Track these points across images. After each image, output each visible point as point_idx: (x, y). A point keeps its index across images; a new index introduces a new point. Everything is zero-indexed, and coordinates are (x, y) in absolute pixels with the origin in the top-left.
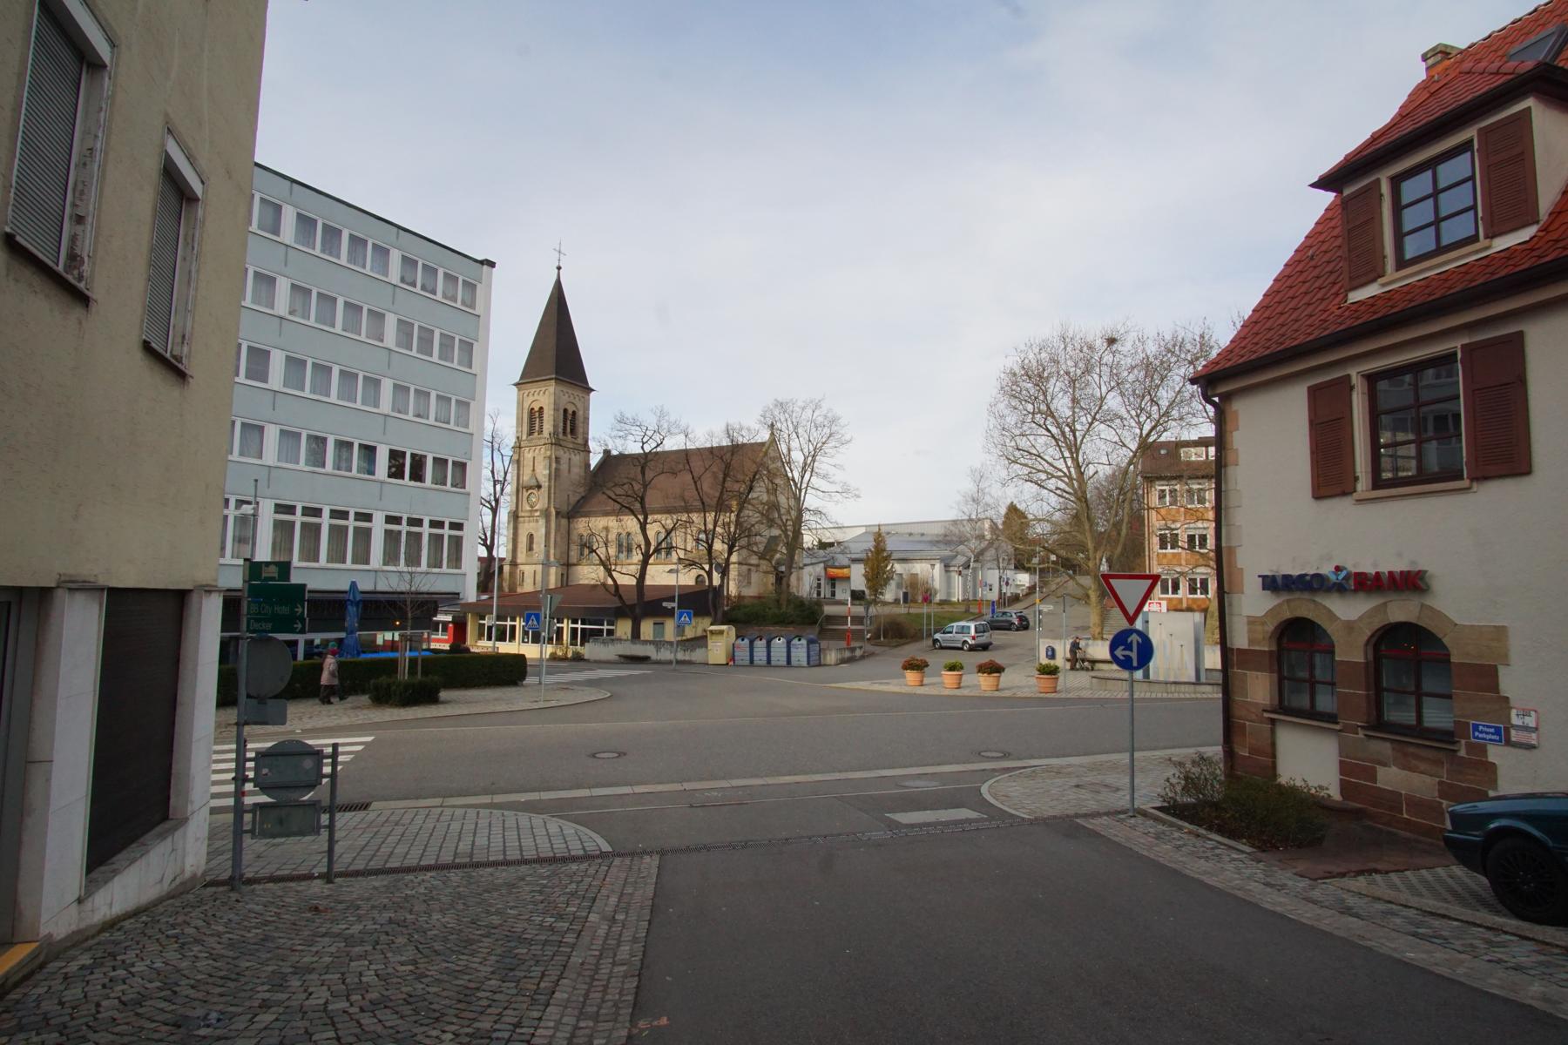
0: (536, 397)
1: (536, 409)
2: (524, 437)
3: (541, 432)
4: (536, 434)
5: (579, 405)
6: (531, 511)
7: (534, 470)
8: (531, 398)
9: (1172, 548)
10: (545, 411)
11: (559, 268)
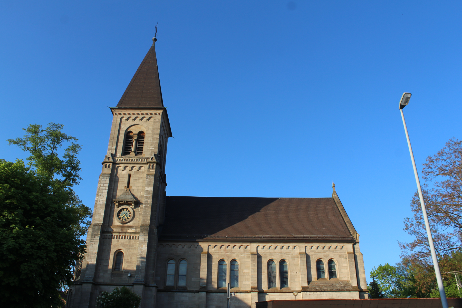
2: (119, 154)
3: (139, 151)
4: (132, 154)
6: (122, 227)
7: (128, 186)
8: (131, 122)
11: (155, 40)
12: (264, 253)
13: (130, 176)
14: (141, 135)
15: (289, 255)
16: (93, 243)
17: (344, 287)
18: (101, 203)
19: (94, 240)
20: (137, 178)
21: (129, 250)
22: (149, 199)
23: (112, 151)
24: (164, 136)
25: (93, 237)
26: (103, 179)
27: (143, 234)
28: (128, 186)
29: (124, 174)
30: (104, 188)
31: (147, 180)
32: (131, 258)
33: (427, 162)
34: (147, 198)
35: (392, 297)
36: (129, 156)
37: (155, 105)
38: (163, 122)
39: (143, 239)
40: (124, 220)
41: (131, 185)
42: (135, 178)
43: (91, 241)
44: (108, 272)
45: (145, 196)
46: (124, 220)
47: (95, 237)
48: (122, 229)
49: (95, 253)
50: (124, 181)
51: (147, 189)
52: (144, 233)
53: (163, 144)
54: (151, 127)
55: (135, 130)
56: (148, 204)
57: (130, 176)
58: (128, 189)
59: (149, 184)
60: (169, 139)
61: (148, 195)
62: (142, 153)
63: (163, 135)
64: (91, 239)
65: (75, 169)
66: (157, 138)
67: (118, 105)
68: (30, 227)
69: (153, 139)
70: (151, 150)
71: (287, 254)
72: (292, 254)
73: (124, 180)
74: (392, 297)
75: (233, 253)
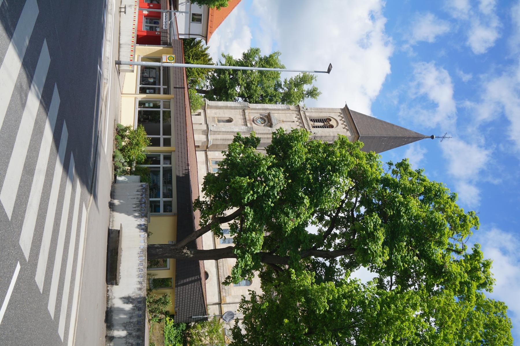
0: (340, 122)
1: (331, 123)
7: (283, 121)
8: (338, 119)
9: (164, 89)
13: (294, 122)
14: (332, 127)
41: (285, 123)
48: (248, 120)
55: (333, 122)
57: (294, 122)
69: (329, 132)
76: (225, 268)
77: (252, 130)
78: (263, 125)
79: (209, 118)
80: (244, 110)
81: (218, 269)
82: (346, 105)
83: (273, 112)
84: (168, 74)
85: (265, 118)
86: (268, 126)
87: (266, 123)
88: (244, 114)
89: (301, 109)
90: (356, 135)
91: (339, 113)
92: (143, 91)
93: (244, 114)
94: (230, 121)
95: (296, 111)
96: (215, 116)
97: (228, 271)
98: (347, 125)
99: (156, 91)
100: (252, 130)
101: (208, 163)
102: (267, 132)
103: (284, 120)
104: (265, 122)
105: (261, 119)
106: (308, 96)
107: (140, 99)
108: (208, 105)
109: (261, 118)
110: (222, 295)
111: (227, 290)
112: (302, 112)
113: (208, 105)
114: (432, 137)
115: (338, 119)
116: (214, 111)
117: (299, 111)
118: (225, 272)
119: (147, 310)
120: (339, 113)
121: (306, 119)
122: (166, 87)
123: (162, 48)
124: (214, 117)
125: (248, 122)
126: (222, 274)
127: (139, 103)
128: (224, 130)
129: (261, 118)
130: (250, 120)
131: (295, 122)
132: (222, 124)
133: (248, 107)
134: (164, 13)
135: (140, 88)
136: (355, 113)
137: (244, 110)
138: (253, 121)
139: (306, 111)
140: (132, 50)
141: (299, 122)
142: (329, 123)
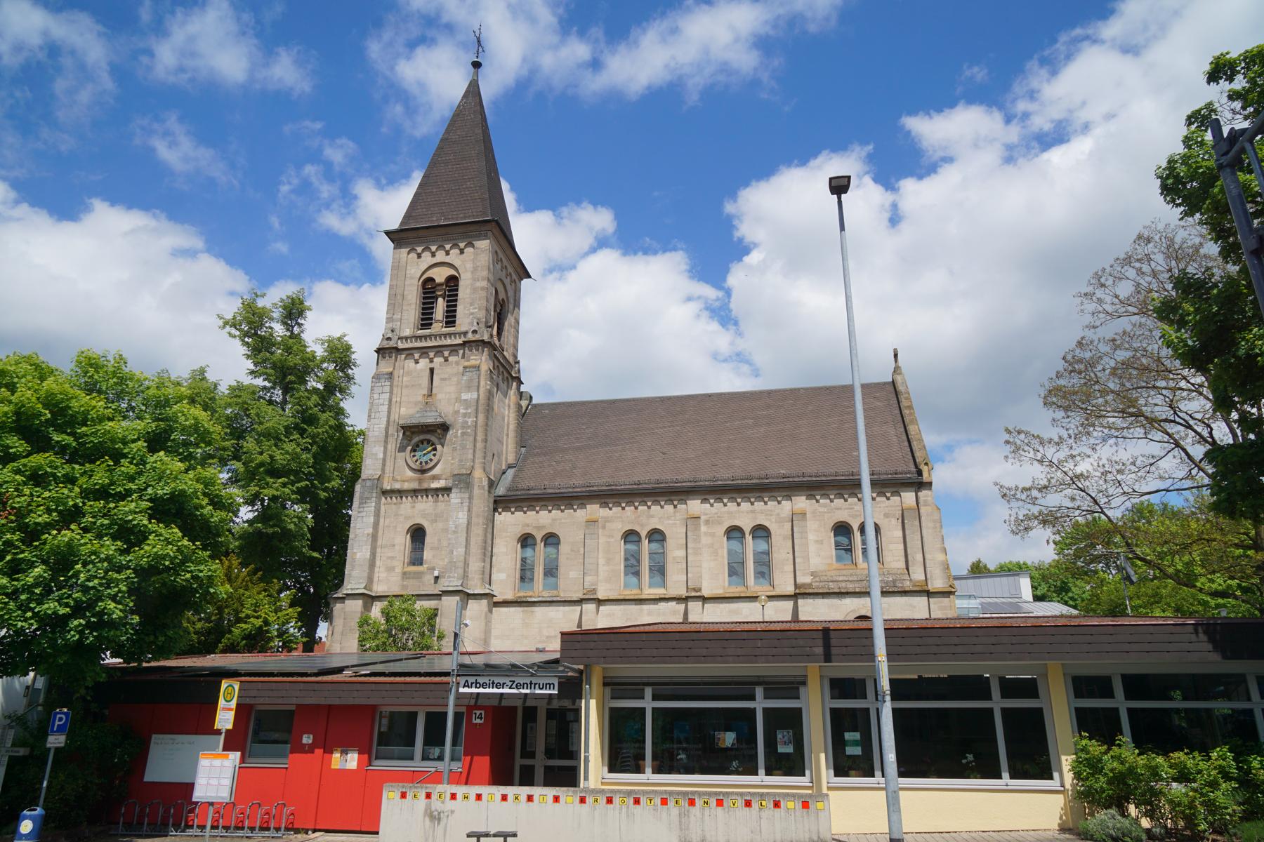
0: (441, 256)
5: (511, 294)
7: (430, 395)
10: (464, 292)
11: (477, 65)
12: (716, 514)
13: (432, 370)
14: (453, 281)
15: (771, 515)
16: (364, 514)
17: (894, 581)
18: (376, 434)
19: (366, 509)
20: (446, 376)
21: (434, 525)
22: (469, 418)
23: (395, 323)
24: (507, 281)
25: (363, 503)
26: (378, 385)
27: (458, 490)
28: (430, 395)
29: (421, 370)
30: (381, 401)
31: (465, 378)
32: (439, 540)
33: (1089, 289)
34: (465, 415)
35: (317, 376)
36: (429, 330)
37: (477, 216)
38: (496, 252)
39: (459, 500)
40: (424, 464)
41: (434, 391)
42: (443, 376)
43: (359, 512)
44: (397, 570)
45: (462, 411)
46: (424, 464)
47: (366, 503)
48: (420, 483)
49: (368, 535)
50: (420, 385)
51: (465, 396)
52: (461, 488)
53: (508, 298)
54: (469, 265)
55: (440, 275)
56: (469, 427)
57: (432, 370)
58: (429, 400)
59: (469, 387)
60: (525, 282)
61: (467, 409)
62: (454, 322)
63: (504, 279)
64: (359, 507)
65: (1157, 313)
66: (482, 289)
67: (402, 223)
68: (199, 593)
69: (475, 290)
70: (472, 314)
71: (767, 515)
72: (778, 514)
73: (420, 382)
74: (317, 376)
75: (652, 516)
76: (841, 579)
77: (464, 477)
78: (439, 447)
79: (404, 587)
80: (385, 493)
81: (847, 593)
82: (388, 233)
83: (394, 416)
84: (698, 684)
85: (416, 439)
86: (444, 435)
87: (433, 439)
88: (400, 493)
89: (392, 344)
90: (488, 226)
91: (409, 253)
92: (792, 764)
93: (400, 493)
94: (418, 534)
95: (396, 358)
96: (399, 570)
97: (844, 572)
98: (455, 242)
99: (792, 721)
100: (464, 477)
101: (530, 600)
102: (471, 439)
103: (425, 392)
104: (429, 441)
105: (415, 451)
106: (300, 325)
107: (606, 769)
108: (365, 588)
109: (414, 450)
110: (912, 588)
111: (895, 578)
112: (401, 345)
113: (365, 588)
114: (477, 65)
115: (427, 259)
116: (380, 572)
117: (398, 350)
118: (850, 579)
119: (619, 760)
120: (409, 253)
121: (420, 338)
122: (648, 692)
123: (593, 703)
124: (404, 573)
125: (425, 486)
126: (857, 585)
127: (659, 773)
128: (462, 550)
129: (414, 450)
130: (420, 481)
131: (432, 365)
132: (427, 555)
133: (378, 479)
134: (461, 690)
135: (657, 770)
136: (408, 216)
137: (385, 493)
138: (423, 471)
139: (397, 332)
140: (523, 798)
141: (420, 357)
142: (441, 284)
